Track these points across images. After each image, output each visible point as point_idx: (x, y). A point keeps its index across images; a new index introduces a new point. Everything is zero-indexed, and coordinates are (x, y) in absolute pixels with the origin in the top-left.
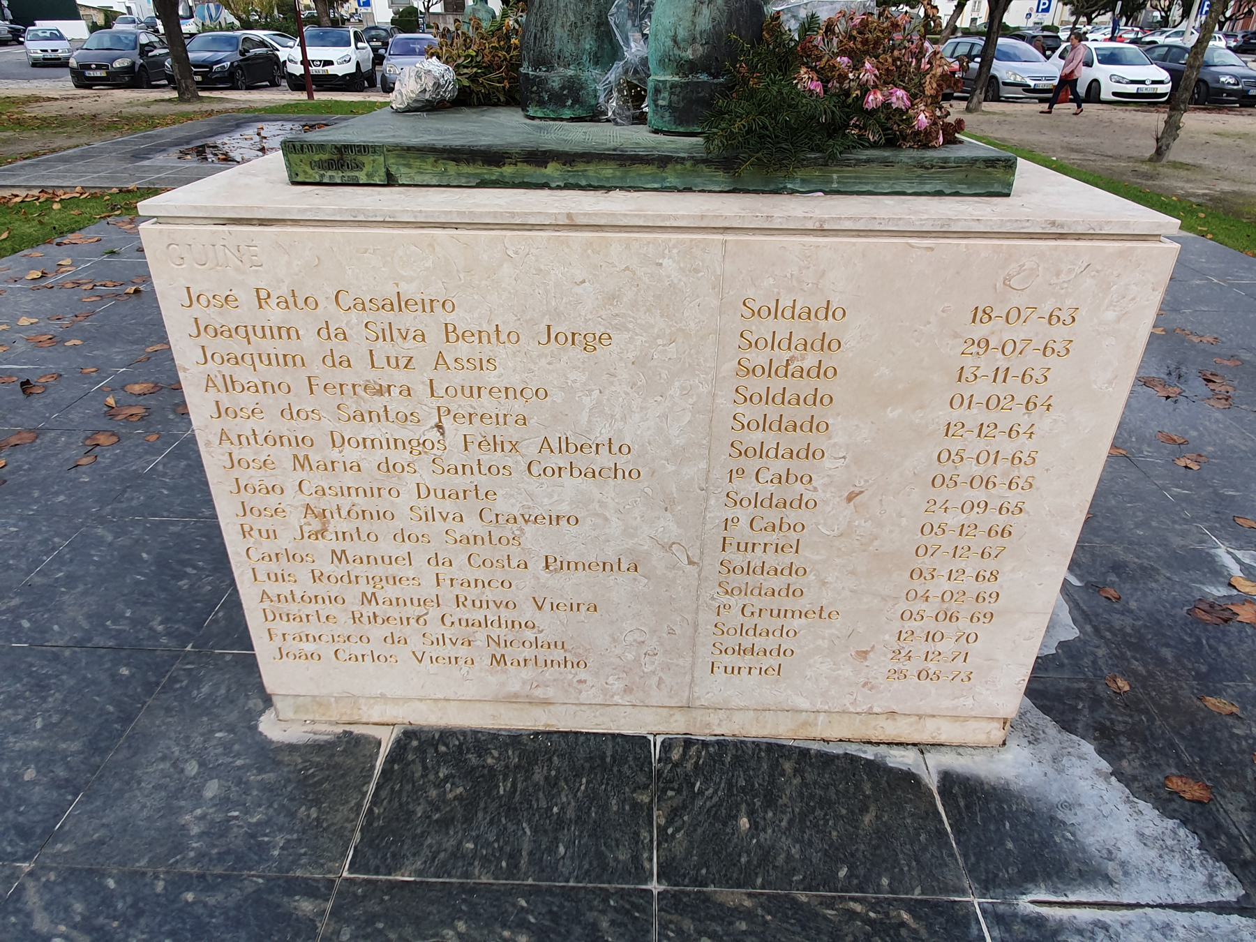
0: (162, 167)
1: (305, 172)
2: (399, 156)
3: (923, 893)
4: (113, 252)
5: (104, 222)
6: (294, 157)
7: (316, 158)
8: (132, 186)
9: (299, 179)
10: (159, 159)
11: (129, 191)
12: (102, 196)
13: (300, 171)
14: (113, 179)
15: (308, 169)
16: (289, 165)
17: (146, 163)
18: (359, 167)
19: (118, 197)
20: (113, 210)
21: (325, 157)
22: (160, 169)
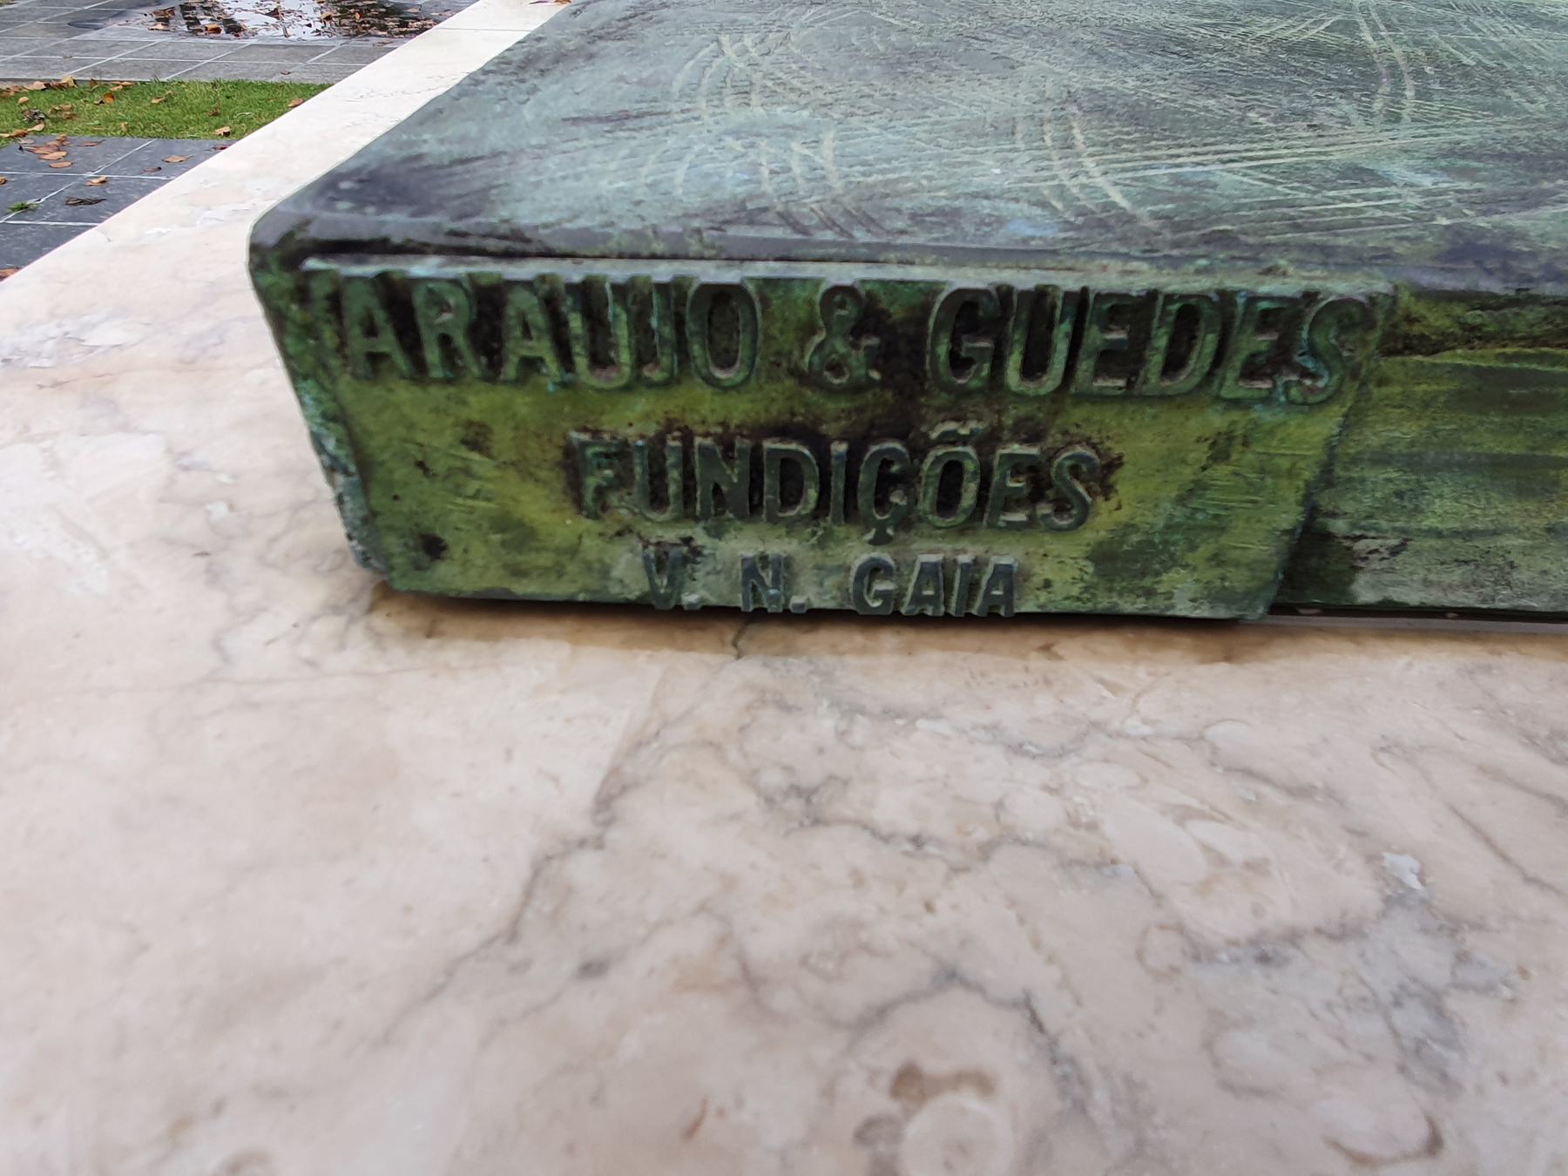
0: (116, 44)
1: (516, 533)
2: (1485, 393)
3: (701, 448)
4: (24, 208)
5: (14, 145)
6: (411, 412)
7: (635, 419)
8: (66, 78)
9: (448, 575)
10: (113, 31)
11: (61, 87)
12: (18, 94)
13: (452, 515)
14: (36, 64)
15: (538, 505)
16: (353, 460)
17: (92, 35)
18: (1051, 492)
19: (43, 97)
20: (31, 122)
21: (716, 404)
22: (113, 47)
